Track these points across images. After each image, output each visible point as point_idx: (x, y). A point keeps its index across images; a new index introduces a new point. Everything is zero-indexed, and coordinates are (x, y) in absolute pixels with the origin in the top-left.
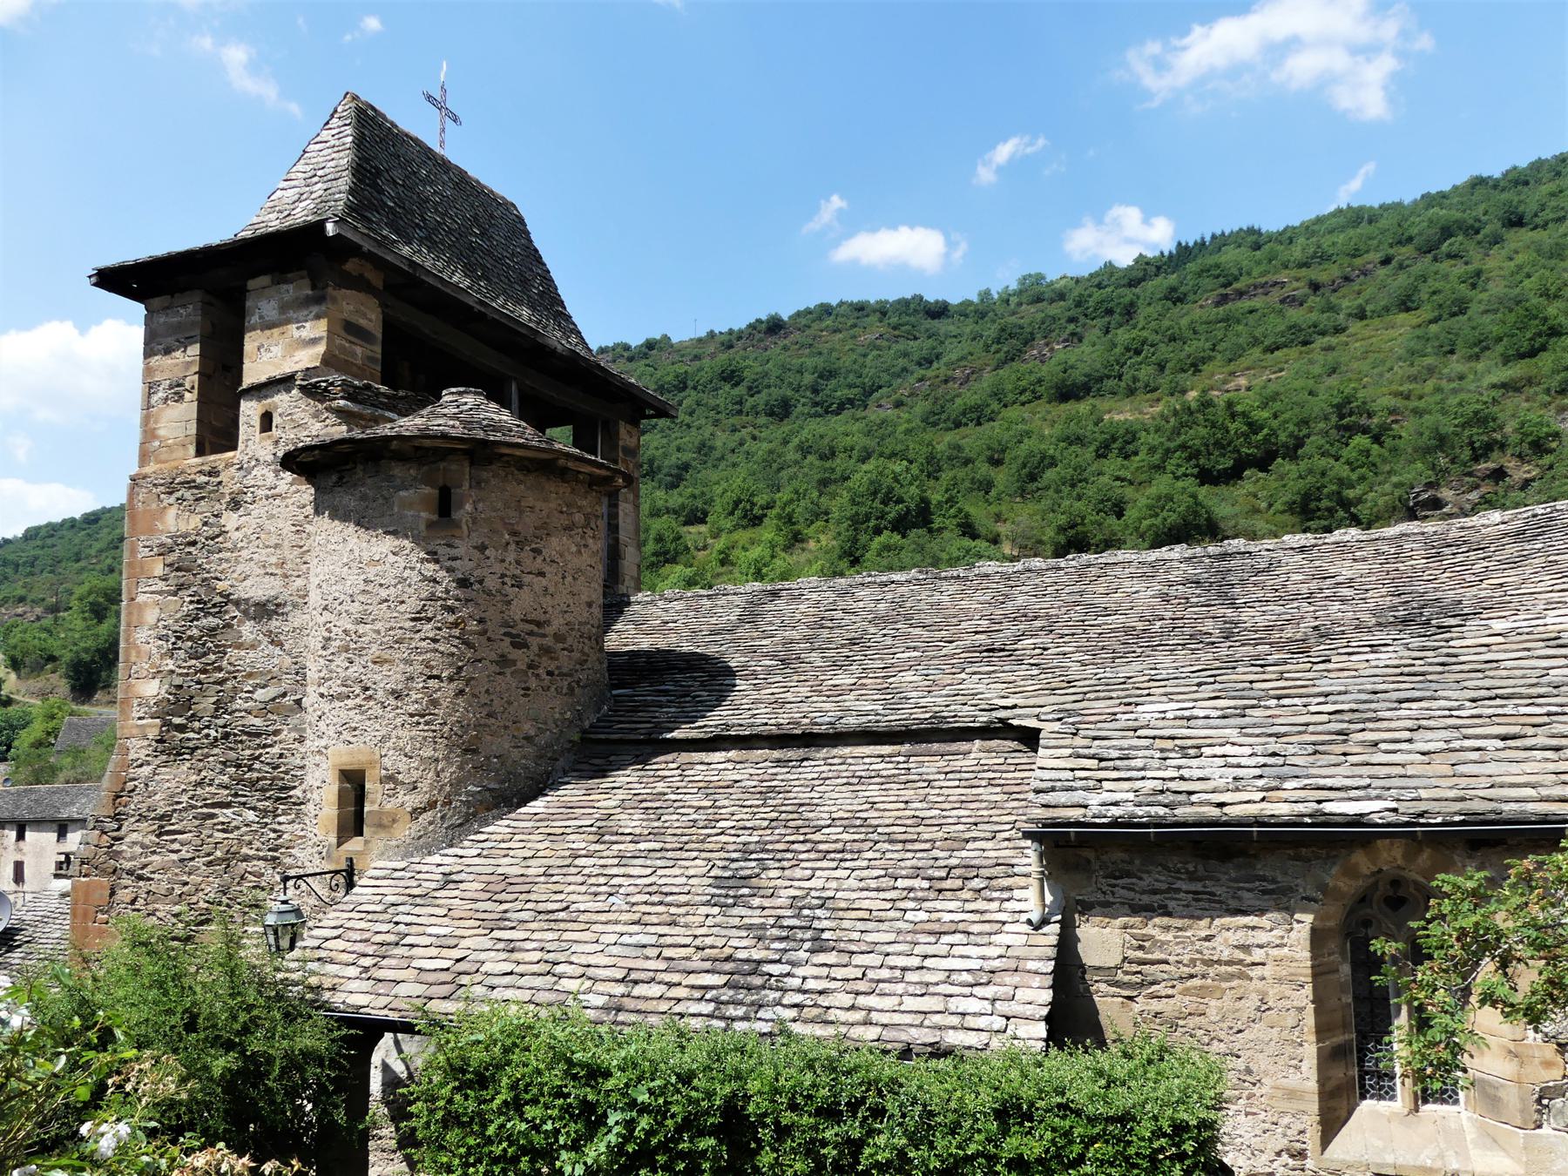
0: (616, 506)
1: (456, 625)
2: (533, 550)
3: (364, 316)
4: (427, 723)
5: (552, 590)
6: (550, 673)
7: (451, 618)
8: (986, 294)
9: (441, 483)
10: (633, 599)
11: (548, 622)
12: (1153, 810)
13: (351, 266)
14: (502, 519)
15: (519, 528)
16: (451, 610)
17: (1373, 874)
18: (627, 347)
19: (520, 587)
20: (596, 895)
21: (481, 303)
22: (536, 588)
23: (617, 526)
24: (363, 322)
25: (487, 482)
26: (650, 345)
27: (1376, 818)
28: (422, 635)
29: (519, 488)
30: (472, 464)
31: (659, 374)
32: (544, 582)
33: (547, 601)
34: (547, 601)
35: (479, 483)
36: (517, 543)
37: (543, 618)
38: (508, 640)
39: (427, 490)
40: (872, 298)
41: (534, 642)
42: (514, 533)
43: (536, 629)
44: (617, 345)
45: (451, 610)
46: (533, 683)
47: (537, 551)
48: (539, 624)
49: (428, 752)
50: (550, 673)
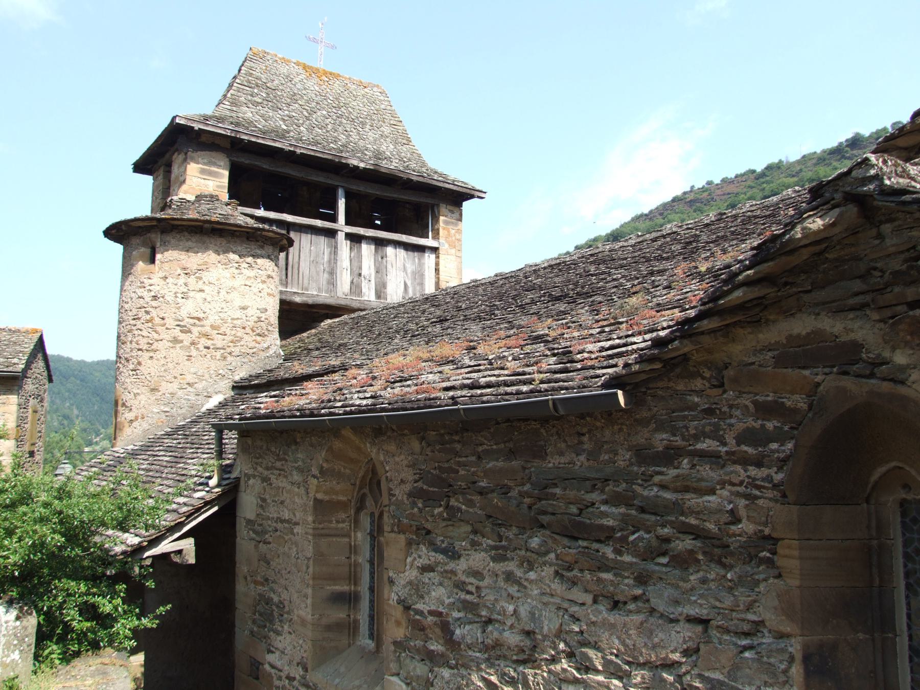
2: (197, 278)
5: (208, 300)
7: (148, 317)
8: (780, 161)
10: (717, 492)
12: (488, 379)
18: (754, 171)
25: (169, 242)
26: (769, 168)
33: (206, 307)
37: (201, 315)
38: (178, 328)
39: (143, 249)
40: (439, 171)
41: (195, 330)
45: (147, 313)
46: (194, 353)
47: (201, 278)
48: (199, 319)
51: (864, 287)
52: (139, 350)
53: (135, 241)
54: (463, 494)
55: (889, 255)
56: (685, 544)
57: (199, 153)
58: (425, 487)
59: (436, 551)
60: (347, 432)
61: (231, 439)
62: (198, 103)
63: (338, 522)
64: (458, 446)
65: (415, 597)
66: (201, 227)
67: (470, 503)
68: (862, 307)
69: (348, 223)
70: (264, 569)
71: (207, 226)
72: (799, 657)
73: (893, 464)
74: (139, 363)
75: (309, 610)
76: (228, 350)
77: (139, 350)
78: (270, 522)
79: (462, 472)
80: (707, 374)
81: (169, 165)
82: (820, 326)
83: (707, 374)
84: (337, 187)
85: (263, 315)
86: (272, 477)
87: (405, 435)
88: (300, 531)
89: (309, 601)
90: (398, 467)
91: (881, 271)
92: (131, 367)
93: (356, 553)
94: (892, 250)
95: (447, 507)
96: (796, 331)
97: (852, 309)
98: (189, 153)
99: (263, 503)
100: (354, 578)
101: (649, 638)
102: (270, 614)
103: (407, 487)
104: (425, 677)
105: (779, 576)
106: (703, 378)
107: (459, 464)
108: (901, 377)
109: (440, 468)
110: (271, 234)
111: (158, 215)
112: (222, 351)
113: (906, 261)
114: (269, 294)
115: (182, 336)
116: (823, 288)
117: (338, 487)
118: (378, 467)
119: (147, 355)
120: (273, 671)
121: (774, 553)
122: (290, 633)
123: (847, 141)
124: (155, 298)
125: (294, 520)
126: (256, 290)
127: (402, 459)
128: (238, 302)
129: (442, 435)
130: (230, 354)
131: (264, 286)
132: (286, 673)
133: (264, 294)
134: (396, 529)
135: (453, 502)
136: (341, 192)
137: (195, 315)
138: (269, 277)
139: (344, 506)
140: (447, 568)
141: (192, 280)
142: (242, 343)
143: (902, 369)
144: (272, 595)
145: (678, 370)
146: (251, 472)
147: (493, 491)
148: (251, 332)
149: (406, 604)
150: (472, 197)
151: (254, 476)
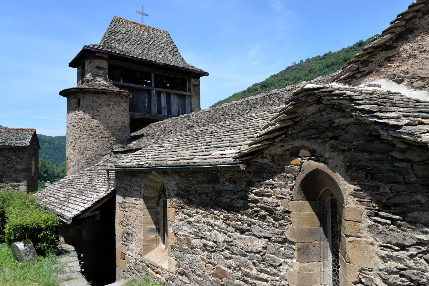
3: (102, 64)
7: (79, 126)
16: (78, 124)
18: (319, 57)
20: (362, 202)
26: (326, 55)
29: (94, 97)
30: (82, 94)
31: (327, 62)
32: (100, 117)
39: (75, 100)
42: (92, 107)
44: (317, 56)
45: (78, 124)
47: (98, 111)
51: (317, 132)
53: (72, 97)
54: (193, 195)
55: (324, 122)
56: (263, 213)
57: (95, 60)
58: (181, 192)
59: (184, 214)
60: (154, 173)
61: (113, 175)
62: (95, 39)
63: (152, 204)
64: (191, 179)
66: (98, 91)
67: (195, 198)
68: (316, 138)
69: (156, 87)
71: (100, 91)
72: (296, 249)
73: (327, 188)
74: (76, 144)
75: (142, 234)
76: (111, 138)
79: (193, 187)
80: (269, 158)
81: (83, 65)
82: (303, 143)
83: (269, 158)
86: (128, 188)
89: (142, 232)
90: (171, 185)
91: (322, 127)
92: (73, 145)
93: (158, 214)
94: (325, 120)
95: (188, 199)
96: (296, 145)
97: (313, 139)
98: (92, 60)
101: (252, 243)
103: (175, 192)
105: (291, 224)
106: (268, 159)
107: (192, 185)
108: (327, 161)
109: (185, 186)
110: (125, 93)
111: (80, 87)
113: (329, 124)
114: (125, 116)
115: (93, 133)
116: (305, 131)
117: (152, 192)
118: (165, 185)
119: (78, 141)
120: (130, 257)
121: (289, 216)
123: (357, 43)
124: (81, 119)
127: (173, 183)
128: (114, 120)
129: (186, 175)
133: (124, 116)
135: (190, 197)
136: (152, 75)
137: (97, 125)
138: (125, 110)
139: (154, 198)
140: (189, 220)
141: (95, 112)
143: (327, 159)
145: (260, 156)
146: (120, 186)
147: (203, 194)
150: (203, 75)
151: (121, 188)
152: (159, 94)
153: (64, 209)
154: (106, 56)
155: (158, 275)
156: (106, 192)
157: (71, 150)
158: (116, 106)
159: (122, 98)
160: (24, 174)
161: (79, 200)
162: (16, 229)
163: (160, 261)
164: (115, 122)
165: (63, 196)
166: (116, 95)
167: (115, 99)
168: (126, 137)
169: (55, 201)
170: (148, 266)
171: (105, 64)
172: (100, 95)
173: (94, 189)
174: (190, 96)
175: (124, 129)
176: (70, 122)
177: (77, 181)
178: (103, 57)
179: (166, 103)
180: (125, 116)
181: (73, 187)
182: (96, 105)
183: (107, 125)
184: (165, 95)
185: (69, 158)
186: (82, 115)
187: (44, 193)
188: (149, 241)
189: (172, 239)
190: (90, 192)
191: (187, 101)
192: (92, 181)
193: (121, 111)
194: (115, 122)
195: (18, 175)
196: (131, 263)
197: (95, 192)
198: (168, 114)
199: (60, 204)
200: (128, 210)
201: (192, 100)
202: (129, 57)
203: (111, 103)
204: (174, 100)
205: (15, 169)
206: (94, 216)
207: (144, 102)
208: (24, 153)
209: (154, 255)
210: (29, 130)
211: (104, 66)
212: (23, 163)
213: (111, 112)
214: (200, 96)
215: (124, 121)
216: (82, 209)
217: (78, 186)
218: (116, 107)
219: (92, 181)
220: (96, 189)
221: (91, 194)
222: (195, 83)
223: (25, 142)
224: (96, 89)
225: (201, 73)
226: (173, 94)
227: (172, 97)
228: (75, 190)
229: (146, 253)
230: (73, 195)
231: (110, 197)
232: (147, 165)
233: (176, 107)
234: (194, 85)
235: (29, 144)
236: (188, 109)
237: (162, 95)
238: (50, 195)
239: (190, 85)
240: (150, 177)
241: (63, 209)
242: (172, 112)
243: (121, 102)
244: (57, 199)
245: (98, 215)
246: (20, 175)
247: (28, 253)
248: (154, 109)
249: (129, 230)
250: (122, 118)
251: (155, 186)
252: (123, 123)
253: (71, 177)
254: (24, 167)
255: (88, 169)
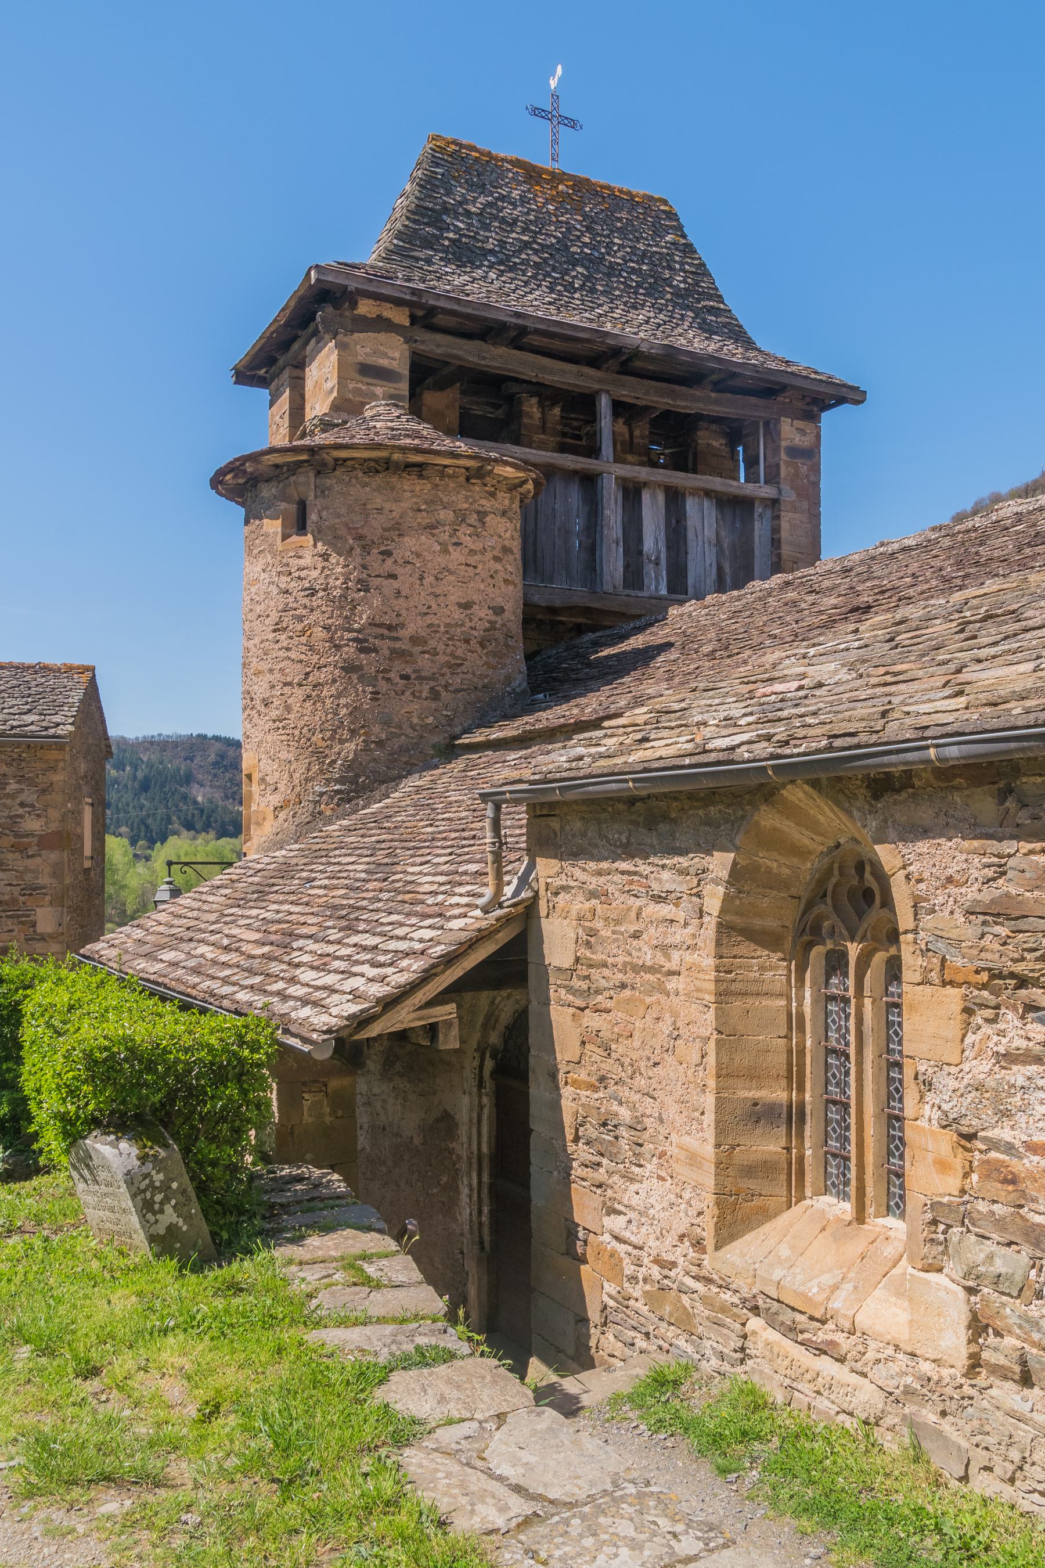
0: (778, 517)
1: (303, 632)
2: (382, 553)
3: (385, 355)
4: (284, 728)
6: (405, 677)
9: (297, 498)
11: (403, 626)
13: (365, 308)
14: (347, 525)
15: (364, 531)
16: (300, 619)
17: (831, 850)
19: (367, 591)
21: (518, 315)
22: (386, 591)
23: (779, 541)
24: (384, 362)
25: (329, 489)
27: (743, 753)
28: (279, 645)
32: (396, 584)
34: (400, 604)
35: (323, 492)
36: (364, 547)
42: (360, 538)
43: (386, 632)
45: (300, 619)
46: (383, 686)
47: (388, 553)
48: (390, 628)
49: (284, 755)
50: (405, 677)
52: (286, 684)
60: (796, 794)
65: (988, 1115)
69: (617, 460)
70: (599, 1059)
71: (396, 456)
74: (288, 709)
75: (710, 1135)
77: (286, 684)
78: (606, 972)
84: (598, 392)
85: (498, 619)
87: (957, 788)
88: (681, 987)
92: (274, 714)
99: (590, 938)
100: (794, 1077)
102: (626, 1142)
104: (1018, 1278)
112: (432, 684)
114: (506, 581)
117: (765, 903)
119: (299, 693)
120: (622, 1248)
122: (661, 1178)
125: (668, 966)
126: (484, 574)
130: (446, 687)
131: (498, 566)
132: (654, 1253)
133: (499, 577)
134: (934, 976)
138: (506, 550)
141: (374, 559)
142: (463, 669)
144: (615, 1107)
148: (479, 649)
149: (965, 1130)
150: (841, 401)
152: (632, 492)
153: (278, 993)
154: (400, 317)
155: (825, 1365)
156: (486, 911)
157: (269, 738)
158: (464, 529)
159: (493, 495)
160: (53, 856)
161: (344, 951)
162: (102, 1067)
163: (835, 1288)
164: (460, 605)
165: (257, 936)
166: (468, 480)
167: (460, 500)
168: (508, 680)
169: (224, 958)
170: (755, 1310)
171: (397, 355)
172: (394, 480)
173: (410, 902)
174: (774, 503)
175: (502, 641)
176: (258, 609)
177: (304, 874)
178: (388, 321)
179: (662, 537)
180: (506, 581)
181: (293, 898)
182: (378, 522)
183: (429, 619)
184: (661, 498)
185: (256, 777)
186: (315, 574)
187: (161, 929)
188: (749, 1171)
189: (942, 1166)
190: (394, 918)
191: (760, 529)
192: (383, 870)
193: (489, 555)
194: (460, 605)
195: (29, 862)
196: (633, 1279)
197: (416, 914)
198: (671, 589)
199: (251, 972)
200: (609, 1004)
201: (785, 525)
202: (502, 318)
203: (446, 515)
204: (702, 521)
205: (17, 835)
206: (432, 1030)
207: (567, 533)
208: (53, 769)
209: (784, 1251)
210: (70, 668)
211: (394, 365)
212: (50, 811)
213: (442, 560)
214: (817, 504)
215: (499, 601)
216: (377, 990)
217: (321, 892)
218: (464, 534)
219: (383, 870)
220: (422, 902)
221: (402, 925)
222: (798, 440)
223: (57, 719)
224: (378, 446)
225: (830, 390)
226: (696, 492)
227: (691, 505)
228: (307, 910)
229: (732, 1237)
230: (304, 930)
231: (503, 937)
232: (763, 749)
233: (711, 558)
234: (794, 452)
235: (71, 728)
236: (759, 562)
237: (646, 496)
238: (190, 934)
239: (776, 451)
240: (767, 818)
241: (272, 994)
242: (690, 581)
243: (485, 514)
244: (227, 949)
245: (449, 1024)
246: (38, 860)
247: (158, 1198)
248: (613, 564)
249: (615, 1107)
250: (490, 590)
251: (786, 871)
252: (496, 614)
253: (267, 860)
254: (54, 826)
255: (345, 822)
